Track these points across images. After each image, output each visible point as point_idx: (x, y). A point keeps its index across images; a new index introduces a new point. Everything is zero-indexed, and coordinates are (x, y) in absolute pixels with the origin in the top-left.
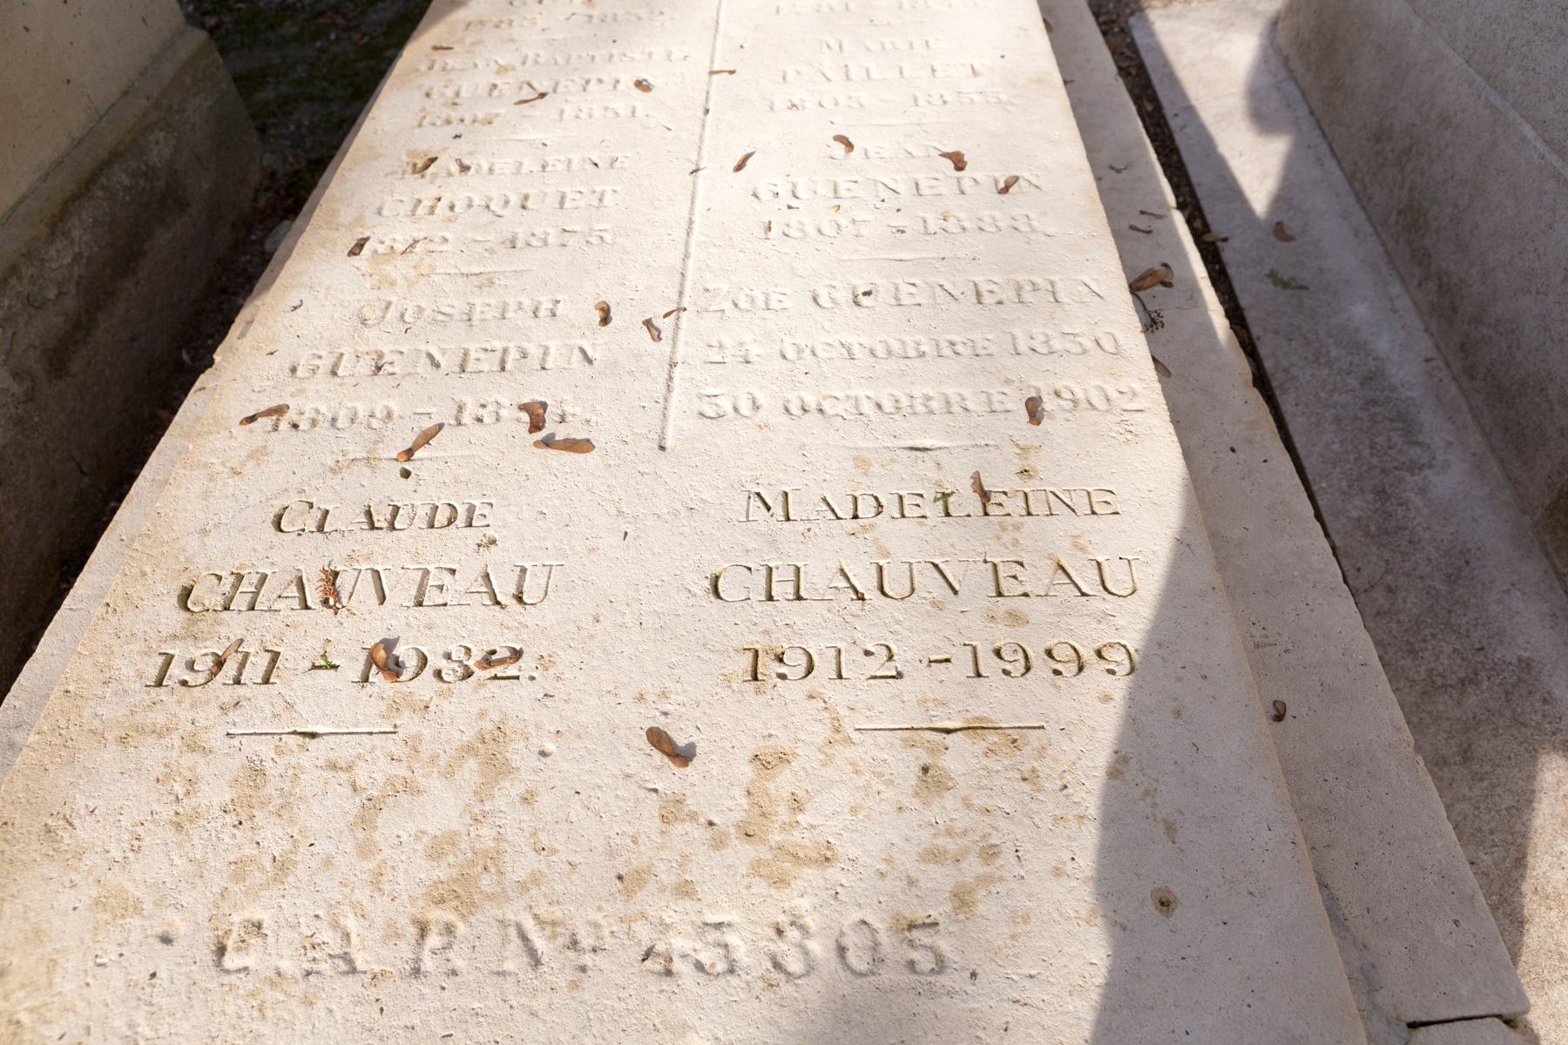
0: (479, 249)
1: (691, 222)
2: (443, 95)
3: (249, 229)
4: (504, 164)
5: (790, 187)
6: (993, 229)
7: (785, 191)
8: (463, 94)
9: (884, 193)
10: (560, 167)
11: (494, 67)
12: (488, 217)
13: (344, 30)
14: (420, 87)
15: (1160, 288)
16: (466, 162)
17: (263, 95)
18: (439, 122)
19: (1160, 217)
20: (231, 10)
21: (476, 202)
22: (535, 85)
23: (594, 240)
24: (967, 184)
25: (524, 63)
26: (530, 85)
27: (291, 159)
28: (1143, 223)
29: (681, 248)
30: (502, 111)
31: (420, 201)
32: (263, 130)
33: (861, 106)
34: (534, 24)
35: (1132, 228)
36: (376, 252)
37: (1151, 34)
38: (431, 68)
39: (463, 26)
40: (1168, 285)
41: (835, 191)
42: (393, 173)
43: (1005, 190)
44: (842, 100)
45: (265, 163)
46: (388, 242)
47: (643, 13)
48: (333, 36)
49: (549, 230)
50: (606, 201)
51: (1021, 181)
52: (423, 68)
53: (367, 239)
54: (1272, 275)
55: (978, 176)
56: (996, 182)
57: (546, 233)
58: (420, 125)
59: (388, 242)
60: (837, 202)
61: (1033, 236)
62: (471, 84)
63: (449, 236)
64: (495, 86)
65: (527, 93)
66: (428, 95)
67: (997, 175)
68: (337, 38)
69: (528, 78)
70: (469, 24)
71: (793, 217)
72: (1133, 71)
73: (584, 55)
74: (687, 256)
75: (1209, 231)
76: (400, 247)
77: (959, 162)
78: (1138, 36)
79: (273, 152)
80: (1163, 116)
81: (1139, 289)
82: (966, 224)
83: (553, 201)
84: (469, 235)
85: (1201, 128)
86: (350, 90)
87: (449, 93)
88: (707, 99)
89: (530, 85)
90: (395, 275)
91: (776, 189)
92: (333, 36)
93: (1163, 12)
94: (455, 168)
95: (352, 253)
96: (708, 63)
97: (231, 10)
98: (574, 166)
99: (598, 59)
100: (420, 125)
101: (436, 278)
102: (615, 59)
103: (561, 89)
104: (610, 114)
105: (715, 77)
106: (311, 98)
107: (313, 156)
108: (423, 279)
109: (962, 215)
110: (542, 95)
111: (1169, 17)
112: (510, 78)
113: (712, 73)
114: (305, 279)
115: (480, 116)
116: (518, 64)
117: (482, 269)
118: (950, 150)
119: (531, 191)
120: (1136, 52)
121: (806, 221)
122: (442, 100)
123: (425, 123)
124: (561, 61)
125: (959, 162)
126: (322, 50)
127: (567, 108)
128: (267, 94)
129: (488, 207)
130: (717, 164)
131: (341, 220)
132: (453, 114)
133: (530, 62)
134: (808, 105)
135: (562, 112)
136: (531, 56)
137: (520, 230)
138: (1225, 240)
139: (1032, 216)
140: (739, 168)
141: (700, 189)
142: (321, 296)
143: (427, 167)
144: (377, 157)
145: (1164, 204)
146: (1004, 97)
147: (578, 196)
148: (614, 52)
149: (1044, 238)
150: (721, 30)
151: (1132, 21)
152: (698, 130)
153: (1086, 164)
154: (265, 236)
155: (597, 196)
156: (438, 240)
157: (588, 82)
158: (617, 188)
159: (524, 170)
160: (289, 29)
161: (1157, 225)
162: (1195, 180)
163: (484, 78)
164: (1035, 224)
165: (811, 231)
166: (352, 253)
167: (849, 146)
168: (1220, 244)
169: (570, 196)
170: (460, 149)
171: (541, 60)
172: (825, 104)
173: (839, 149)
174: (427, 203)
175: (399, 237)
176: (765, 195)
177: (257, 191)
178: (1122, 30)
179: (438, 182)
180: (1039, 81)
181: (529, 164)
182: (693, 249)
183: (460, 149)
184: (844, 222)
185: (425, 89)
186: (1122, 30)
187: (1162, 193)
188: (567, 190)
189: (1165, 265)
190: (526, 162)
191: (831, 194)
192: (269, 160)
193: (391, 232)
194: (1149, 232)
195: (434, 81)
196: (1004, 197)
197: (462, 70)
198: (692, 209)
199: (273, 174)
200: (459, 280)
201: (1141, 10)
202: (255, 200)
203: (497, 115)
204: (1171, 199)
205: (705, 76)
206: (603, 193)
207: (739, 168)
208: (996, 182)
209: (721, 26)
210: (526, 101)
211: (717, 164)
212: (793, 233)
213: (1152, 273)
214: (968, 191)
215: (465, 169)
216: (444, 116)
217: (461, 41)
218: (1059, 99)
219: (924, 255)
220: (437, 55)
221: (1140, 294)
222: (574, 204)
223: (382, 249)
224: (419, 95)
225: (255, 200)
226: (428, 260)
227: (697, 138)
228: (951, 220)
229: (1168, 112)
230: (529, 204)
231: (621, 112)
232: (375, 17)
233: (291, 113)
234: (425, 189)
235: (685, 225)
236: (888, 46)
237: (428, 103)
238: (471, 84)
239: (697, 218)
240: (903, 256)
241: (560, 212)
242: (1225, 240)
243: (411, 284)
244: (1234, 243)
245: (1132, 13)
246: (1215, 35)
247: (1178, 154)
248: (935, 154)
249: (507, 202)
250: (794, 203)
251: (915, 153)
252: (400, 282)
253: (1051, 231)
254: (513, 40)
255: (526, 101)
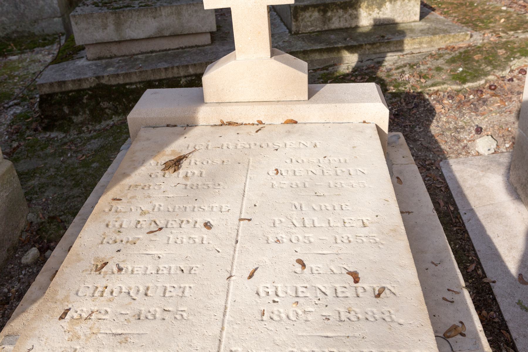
0: (122, 318)
1: (226, 308)
2: (114, 226)
3: (16, 250)
4: (139, 268)
5: (274, 289)
6: (373, 319)
7: (271, 291)
8: (123, 226)
9: (320, 295)
10: (165, 272)
11: (139, 211)
12: (128, 300)
13: (75, 152)
14: (104, 221)
15: (459, 336)
16: (121, 266)
17: (33, 182)
18: (111, 242)
19: (457, 293)
20: (25, 139)
21: (124, 290)
22: (158, 222)
23: (178, 317)
24: (360, 291)
25: (153, 209)
26: (155, 222)
27: (41, 216)
28: (449, 296)
29: (220, 324)
30: (141, 236)
31: (97, 288)
32: (30, 201)
33: (310, 242)
34: (160, 188)
35: (444, 299)
36: (72, 318)
37: (451, 171)
38: (110, 210)
39: (127, 188)
40: (463, 335)
41: (296, 293)
42: (86, 270)
43: (378, 296)
44: (301, 238)
45: (28, 218)
46: (79, 312)
47: (210, 184)
48: (69, 155)
49: (158, 309)
50: (186, 294)
51: (387, 291)
52: (107, 210)
53: (69, 310)
54: (519, 303)
55: (366, 286)
56: (374, 289)
57: (155, 311)
58: (102, 243)
59: (79, 312)
60: (297, 299)
61: (392, 324)
62: (128, 221)
63: (109, 310)
64: (139, 222)
65: (153, 227)
66: (107, 225)
67: (375, 286)
68: (71, 155)
69: (154, 219)
70: (130, 186)
71: (275, 308)
72: (443, 189)
73: (182, 206)
74: (223, 329)
75: (486, 277)
76: (85, 315)
77: (356, 278)
78: (444, 171)
79: (33, 213)
80: (459, 213)
81: (449, 337)
82: (360, 316)
83: (160, 292)
84: (118, 310)
85: (478, 220)
86: (73, 182)
87: (117, 225)
88: (237, 235)
89: (155, 222)
90: (81, 333)
91: (267, 290)
92: (69, 155)
93: (455, 160)
94: (115, 269)
95: (61, 318)
96: (239, 215)
97: (25, 139)
98: (172, 271)
99: (188, 209)
100: (102, 243)
101: (100, 336)
102: (196, 210)
103: (169, 226)
104: (191, 241)
105: (242, 222)
106: (55, 185)
107: (52, 215)
108: (93, 336)
109: (357, 310)
110: (161, 229)
111: (458, 163)
112: (146, 218)
113: (241, 220)
114: (37, 332)
115: (130, 239)
116: (150, 210)
117: (123, 332)
118: (351, 270)
119: (150, 285)
120: (444, 179)
121: (281, 310)
122: (113, 229)
123: (105, 241)
124: (171, 210)
125: (356, 278)
126: (63, 162)
127: (171, 236)
128: (34, 182)
129: (129, 293)
130: (240, 274)
131: (58, 297)
132: (118, 237)
133: (156, 210)
134: (285, 240)
135: (169, 238)
136: (157, 206)
137: (143, 309)
138: (494, 282)
139: (392, 312)
140: (250, 277)
141: (231, 287)
142: (43, 343)
143: (102, 267)
144: (79, 261)
145: (459, 285)
146: (377, 239)
147: (172, 289)
148: (196, 206)
149: (398, 326)
150: (246, 195)
151: (441, 164)
152: (232, 253)
153: (417, 281)
154: (23, 255)
155: (182, 290)
156: (103, 312)
157: (182, 222)
158: (192, 285)
159: (148, 272)
160: (50, 150)
161: (456, 297)
162: (477, 248)
163: (135, 217)
164: (393, 316)
165: (284, 316)
166: (61, 318)
167: (304, 266)
168: (491, 284)
169: (169, 289)
170: (118, 258)
171: (162, 208)
172: (293, 240)
173: (298, 268)
174: (100, 289)
175: (85, 309)
176: (263, 294)
177: (22, 231)
178: (437, 168)
179: (107, 277)
180: (394, 231)
181: (151, 269)
182: (226, 325)
183: (118, 258)
184: (300, 312)
185: (106, 222)
186: (437, 168)
187: (458, 278)
188: (168, 285)
189: (461, 323)
190: (149, 267)
191: (294, 295)
192: (31, 216)
193: (82, 307)
194: (452, 302)
195: (111, 218)
196: (378, 300)
197: (124, 212)
198: (227, 300)
199: (32, 223)
200: (111, 337)
201: (446, 159)
202: (21, 236)
203: (138, 239)
204: (463, 283)
205: (237, 222)
206: (184, 288)
207: (250, 277)
208: (374, 289)
209: (246, 193)
210: (152, 232)
211: (240, 274)
212: (275, 318)
213: (455, 327)
214: (361, 295)
215: (120, 270)
216: (113, 238)
217: (126, 196)
218: (403, 242)
219: (339, 334)
220: (114, 203)
221: (450, 340)
222: (170, 294)
223: (76, 316)
224: (103, 225)
225: (21, 236)
226: (97, 324)
227: (231, 258)
228: (352, 313)
229: (462, 212)
230: (149, 293)
231: (197, 240)
232: (89, 147)
233: (44, 192)
234: (100, 281)
235: (222, 310)
236: (323, 208)
237: (107, 230)
238: (128, 221)
239: (229, 306)
240: (329, 334)
241: (163, 299)
242: (494, 282)
243: (88, 339)
244: (498, 284)
245: (441, 161)
246: (481, 174)
247: (468, 234)
248: (344, 272)
249: (138, 291)
250: (276, 299)
251: (335, 271)
252: (82, 337)
253: (401, 321)
254: (149, 197)
255: (152, 232)
